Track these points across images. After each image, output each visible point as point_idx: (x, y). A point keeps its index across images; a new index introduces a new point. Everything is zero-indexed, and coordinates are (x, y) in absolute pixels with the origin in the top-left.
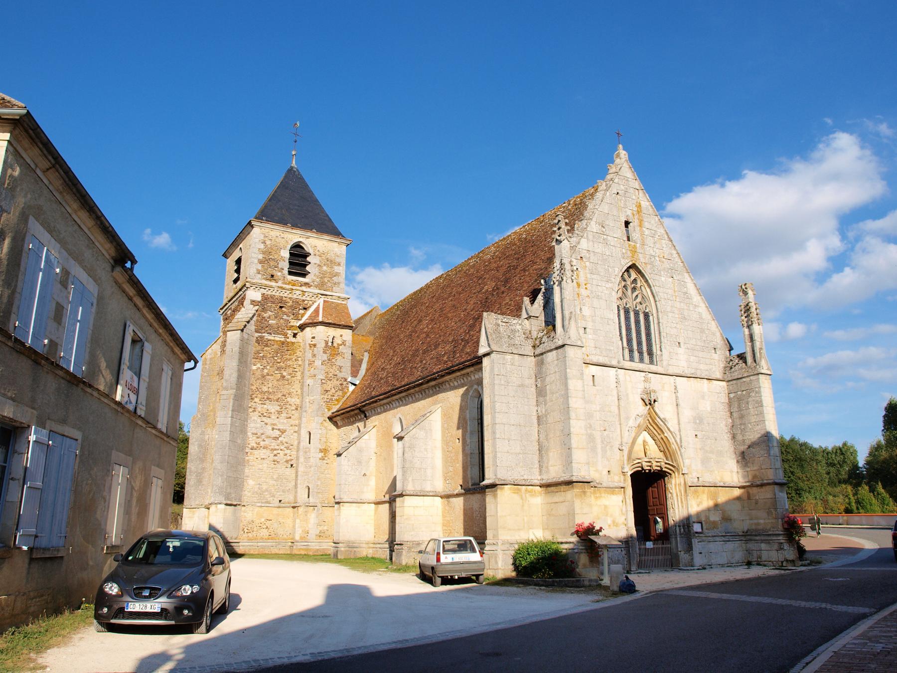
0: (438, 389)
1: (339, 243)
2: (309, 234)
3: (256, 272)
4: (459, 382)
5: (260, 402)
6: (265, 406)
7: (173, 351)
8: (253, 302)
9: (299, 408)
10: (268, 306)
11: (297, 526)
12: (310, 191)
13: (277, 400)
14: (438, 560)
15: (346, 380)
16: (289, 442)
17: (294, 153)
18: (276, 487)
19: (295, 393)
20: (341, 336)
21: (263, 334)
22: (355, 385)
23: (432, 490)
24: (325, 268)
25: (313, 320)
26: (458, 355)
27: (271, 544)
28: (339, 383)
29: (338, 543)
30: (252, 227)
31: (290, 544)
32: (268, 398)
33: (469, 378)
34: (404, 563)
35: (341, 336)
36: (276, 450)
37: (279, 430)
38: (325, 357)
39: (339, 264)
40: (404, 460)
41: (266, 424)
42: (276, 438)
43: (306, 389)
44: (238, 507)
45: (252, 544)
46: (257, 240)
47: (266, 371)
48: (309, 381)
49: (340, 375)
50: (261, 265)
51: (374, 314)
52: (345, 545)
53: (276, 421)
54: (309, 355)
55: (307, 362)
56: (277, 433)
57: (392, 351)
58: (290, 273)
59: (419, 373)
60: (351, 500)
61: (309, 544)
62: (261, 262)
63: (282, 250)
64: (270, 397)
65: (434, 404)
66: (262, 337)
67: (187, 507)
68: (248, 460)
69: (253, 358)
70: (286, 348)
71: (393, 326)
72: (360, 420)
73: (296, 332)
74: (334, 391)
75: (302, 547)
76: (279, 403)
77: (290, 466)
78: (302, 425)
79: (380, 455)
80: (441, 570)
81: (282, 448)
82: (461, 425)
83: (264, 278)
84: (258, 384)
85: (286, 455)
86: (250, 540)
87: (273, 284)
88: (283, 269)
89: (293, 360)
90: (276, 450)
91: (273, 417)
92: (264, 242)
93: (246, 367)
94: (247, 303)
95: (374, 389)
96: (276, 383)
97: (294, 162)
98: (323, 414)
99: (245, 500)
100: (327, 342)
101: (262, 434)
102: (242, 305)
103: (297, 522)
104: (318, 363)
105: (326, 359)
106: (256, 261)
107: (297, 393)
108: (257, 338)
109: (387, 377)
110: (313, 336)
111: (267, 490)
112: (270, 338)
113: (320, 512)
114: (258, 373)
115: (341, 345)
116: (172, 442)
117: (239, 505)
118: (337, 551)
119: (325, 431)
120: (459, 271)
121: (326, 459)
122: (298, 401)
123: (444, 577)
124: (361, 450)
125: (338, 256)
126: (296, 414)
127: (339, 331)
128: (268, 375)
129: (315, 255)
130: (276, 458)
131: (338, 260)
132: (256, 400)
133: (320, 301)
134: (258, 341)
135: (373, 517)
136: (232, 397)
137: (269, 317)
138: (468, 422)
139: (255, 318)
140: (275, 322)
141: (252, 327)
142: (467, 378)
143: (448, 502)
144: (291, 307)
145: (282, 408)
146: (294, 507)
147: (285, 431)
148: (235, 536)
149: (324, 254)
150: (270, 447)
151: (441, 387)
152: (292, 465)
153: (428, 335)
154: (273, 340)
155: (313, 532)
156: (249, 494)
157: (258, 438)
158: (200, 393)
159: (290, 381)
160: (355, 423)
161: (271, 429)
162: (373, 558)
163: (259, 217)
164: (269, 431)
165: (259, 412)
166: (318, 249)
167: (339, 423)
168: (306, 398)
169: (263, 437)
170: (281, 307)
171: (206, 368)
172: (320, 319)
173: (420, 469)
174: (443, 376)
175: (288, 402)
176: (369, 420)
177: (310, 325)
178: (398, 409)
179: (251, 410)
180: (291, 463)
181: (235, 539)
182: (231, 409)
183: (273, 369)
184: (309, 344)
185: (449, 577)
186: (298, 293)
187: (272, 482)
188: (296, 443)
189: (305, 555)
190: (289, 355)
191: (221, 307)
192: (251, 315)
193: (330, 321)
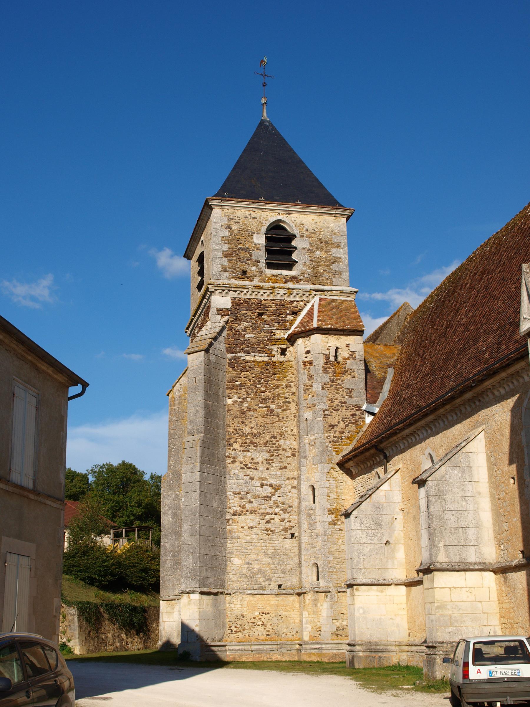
0: (477, 403)
1: (335, 215)
2: (291, 208)
3: (221, 269)
4: (507, 388)
5: (242, 449)
6: (249, 454)
7: (38, 369)
8: (221, 311)
9: (296, 455)
10: (243, 315)
11: (304, 620)
12: (291, 150)
13: (265, 445)
14: (466, 675)
15: (359, 408)
16: (286, 502)
17: (263, 101)
18: (273, 567)
19: (289, 432)
20: (348, 346)
21: (239, 354)
22: (373, 414)
23: (478, 561)
24: (318, 253)
25: (305, 327)
26: (504, 346)
27: (271, 647)
28: (349, 413)
29: (354, 645)
30: (211, 208)
31: (297, 646)
32: (252, 443)
33: (521, 380)
34: (439, 676)
35: (348, 346)
36: (268, 514)
37: (271, 485)
38: (326, 378)
39: (338, 246)
40: (430, 516)
41: (252, 479)
42: (267, 498)
43: (303, 425)
44: (221, 596)
45: (243, 647)
46: (218, 226)
47: (246, 405)
48: (307, 414)
49: (351, 402)
50: (226, 259)
51: (403, 313)
52: (364, 647)
53: (265, 474)
54: (304, 378)
55: (302, 388)
56: (269, 490)
57: (420, 360)
58: (269, 266)
59: (451, 383)
60: (369, 582)
61: (323, 646)
62: (226, 255)
63: (255, 236)
64: (255, 440)
65: (475, 427)
66: (237, 359)
67: (164, 598)
68: (230, 531)
69: (227, 389)
70: (272, 371)
71: (425, 326)
72: (379, 464)
73: (284, 346)
74: (343, 427)
75: (313, 651)
76: (268, 449)
77: (289, 536)
78: (302, 477)
79: (408, 513)
80: (471, 691)
81: (277, 511)
82: (514, 455)
83: (233, 277)
84: (236, 424)
85: (283, 520)
86: (240, 642)
87: (246, 283)
88: (258, 261)
89: (284, 386)
90: (268, 514)
91: (261, 468)
92: (229, 228)
93: (218, 402)
94: (212, 312)
95: (395, 415)
96: (261, 420)
97: (265, 114)
98: (329, 459)
99: (230, 585)
100: (327, 357)
101: (247, 493)
102: (208, 317)
103: (304, 616)
104: (317, 387)
105: (328, 380)
106: (220, 254)
107: (293, 433)
108: (230, 360)
109: (412, 395)
110: (307, 349)
111: (259, 572)
112: (247, 358)
113: (336, 599)
114: (236, 409)
115: (348, 359)
116: (49, 502)
117: (222, 593)
118: (353, 657)
119: (334, 484)
120: (511, 229)
121: (339, 523)
122: (295, 444)
123: (477, 703)
124: (379, 507)
125: (336, 235)
126: (293, 462)
127: (344, 340)
128: (249, 409)
129: (302, 236)
130: (269, 526)
131: (335, 240)
132: (236, 446)
133: (315, 301)
134: (231, 365)
135: (404, 606)
136: (199, 443)
137: (245, 330)
138: (525, 449)
139: (225, 333)
140: (253, 335)
141: (221, 345)
142: (518, 381)
143: (506, 579)
144: (275, 312)
145: (273, 455)
146: (299, 594)
147: (280, 487)
148: (218, 637)
149: (315, 234)
150: (259, 511)
151: (481, 399)
152: (293, 535)
153: (466, 328)
154: (253, 361)
155: (328, 629)
156: (235, 578)
157: (242, 498)
158: (169, 444)
159: (281, 416)
160: (373, 469)
161: (259, 485)
162: (407, 667)
163: (220, 195)
164: (256, 488)
165: (241, 463)
166: (306, 227)
167: (352, 470)
168: (305, 439)
169: (249, 497)
170: (260, 314)
172: (315, 324)
173: (456, 528)
174: (482, 381)
175: (280, 446)
176: (391, 462)
177: (302, 335)
178: (427, 441)
179: (229, 461)
180: (292, 531)
181: (220, 641)
182: (199, 461)
183: (255, 402)
184: (303, 362)
185: (486, 704)
186: (282, 291)
187: (266, 560)
188: (295, 503)
189: (318, 662)
190: (278, 380)
191: (187, 325)
192: (218, 330)
193: (329, 326)
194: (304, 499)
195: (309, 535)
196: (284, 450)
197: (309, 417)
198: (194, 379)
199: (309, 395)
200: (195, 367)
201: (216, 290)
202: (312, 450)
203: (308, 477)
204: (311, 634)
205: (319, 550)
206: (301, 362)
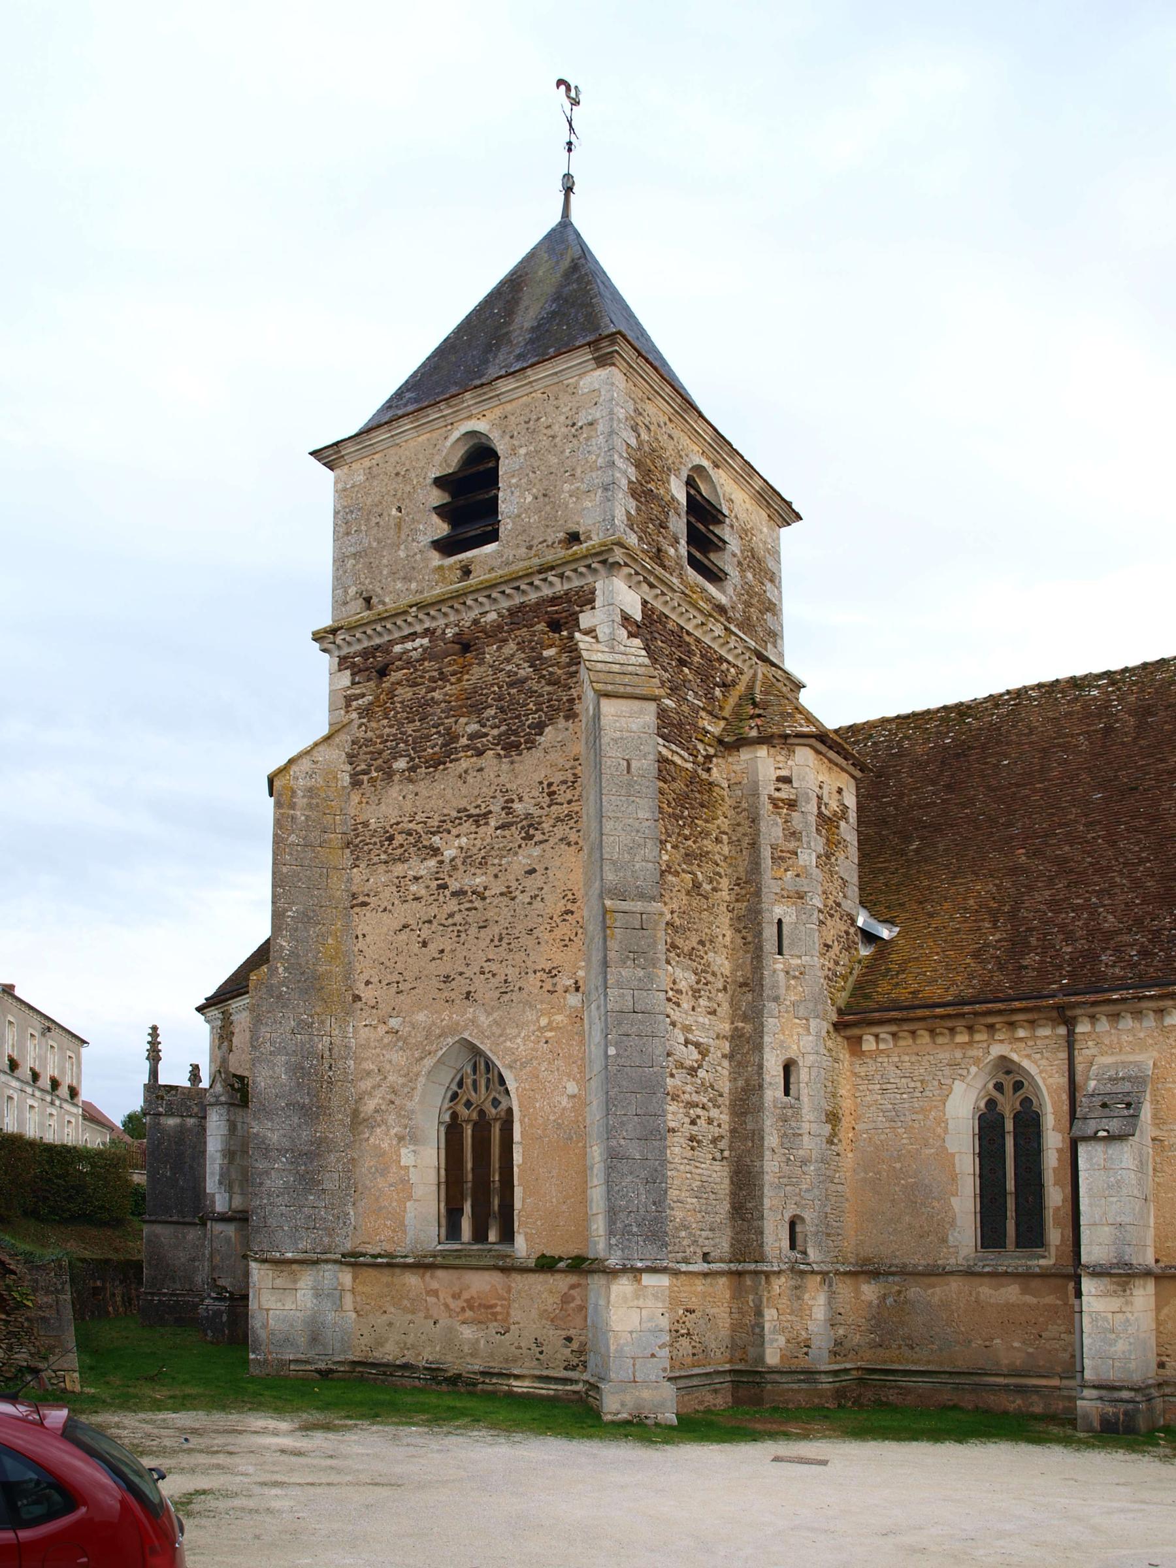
171: (293, 818)
194: (771, 1084)
195: (784, 1159)
196: (714, 974)
197: (788, 917)
198: (625, 763)
199: (786, 870)
200: (626, 734)
201: (626, 565)
202: (795, 988)
203: (782, 1042)
204: (783, 1352)
205: (808, 1190)
206: (766, 797)
